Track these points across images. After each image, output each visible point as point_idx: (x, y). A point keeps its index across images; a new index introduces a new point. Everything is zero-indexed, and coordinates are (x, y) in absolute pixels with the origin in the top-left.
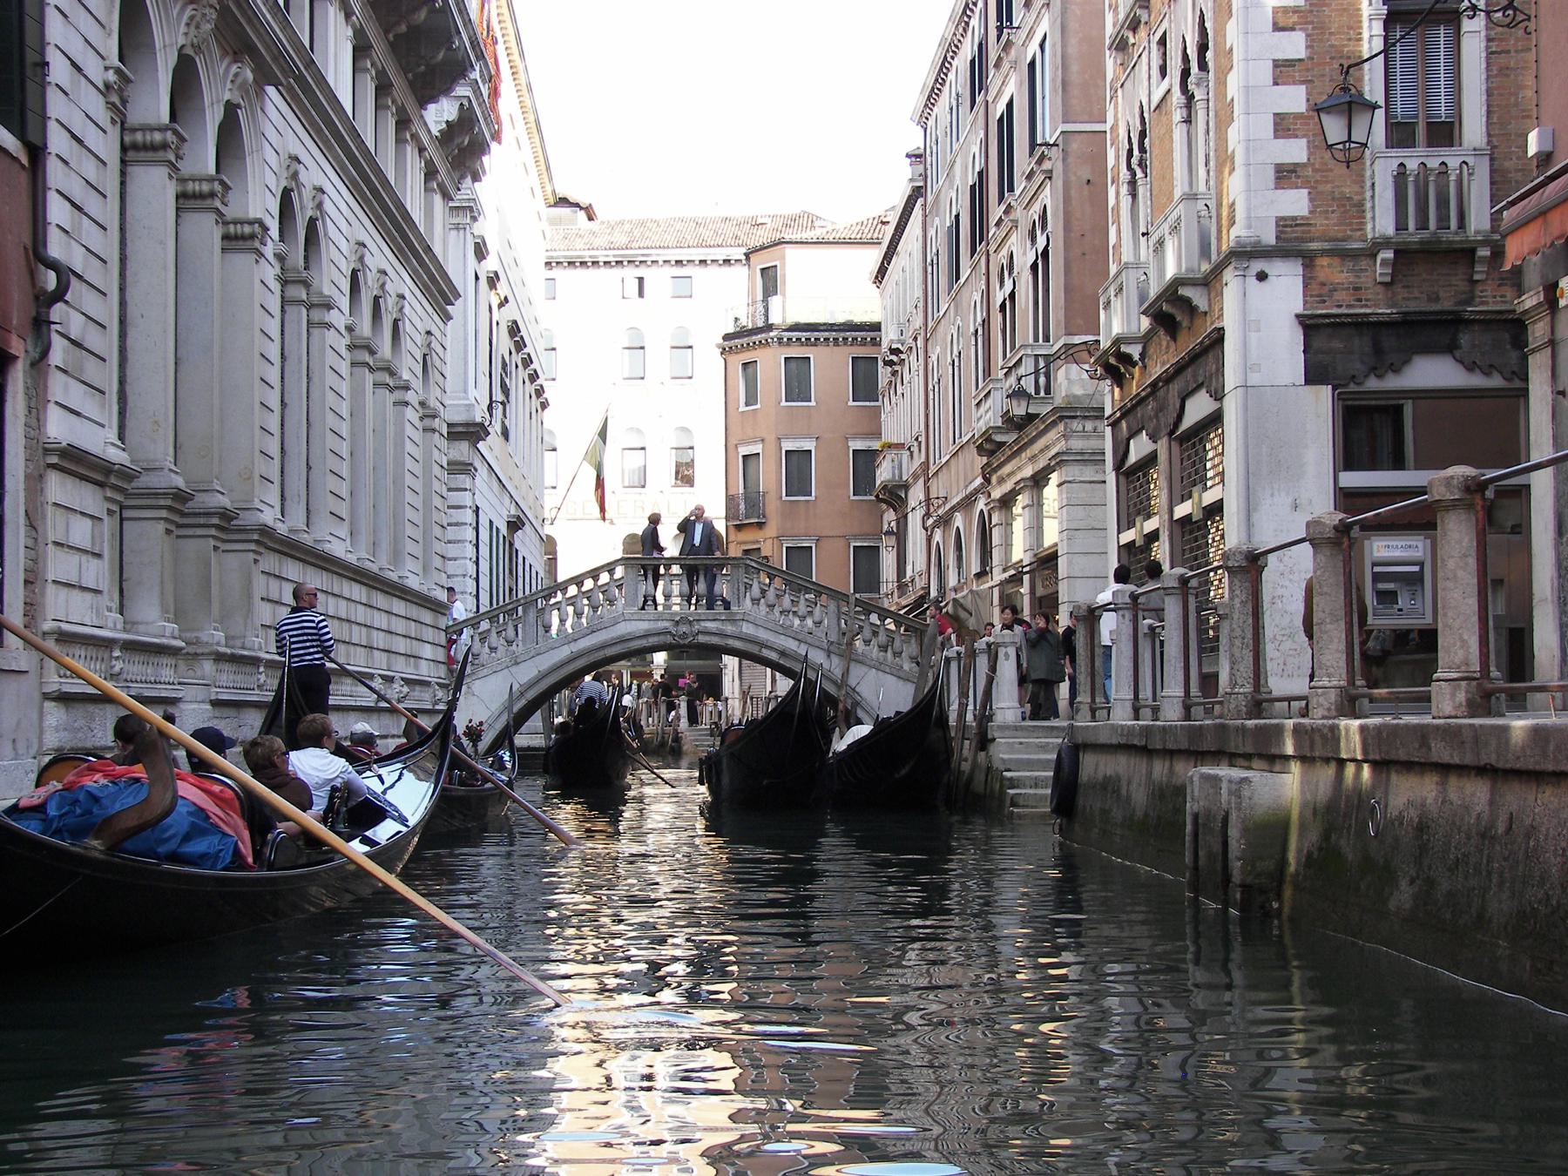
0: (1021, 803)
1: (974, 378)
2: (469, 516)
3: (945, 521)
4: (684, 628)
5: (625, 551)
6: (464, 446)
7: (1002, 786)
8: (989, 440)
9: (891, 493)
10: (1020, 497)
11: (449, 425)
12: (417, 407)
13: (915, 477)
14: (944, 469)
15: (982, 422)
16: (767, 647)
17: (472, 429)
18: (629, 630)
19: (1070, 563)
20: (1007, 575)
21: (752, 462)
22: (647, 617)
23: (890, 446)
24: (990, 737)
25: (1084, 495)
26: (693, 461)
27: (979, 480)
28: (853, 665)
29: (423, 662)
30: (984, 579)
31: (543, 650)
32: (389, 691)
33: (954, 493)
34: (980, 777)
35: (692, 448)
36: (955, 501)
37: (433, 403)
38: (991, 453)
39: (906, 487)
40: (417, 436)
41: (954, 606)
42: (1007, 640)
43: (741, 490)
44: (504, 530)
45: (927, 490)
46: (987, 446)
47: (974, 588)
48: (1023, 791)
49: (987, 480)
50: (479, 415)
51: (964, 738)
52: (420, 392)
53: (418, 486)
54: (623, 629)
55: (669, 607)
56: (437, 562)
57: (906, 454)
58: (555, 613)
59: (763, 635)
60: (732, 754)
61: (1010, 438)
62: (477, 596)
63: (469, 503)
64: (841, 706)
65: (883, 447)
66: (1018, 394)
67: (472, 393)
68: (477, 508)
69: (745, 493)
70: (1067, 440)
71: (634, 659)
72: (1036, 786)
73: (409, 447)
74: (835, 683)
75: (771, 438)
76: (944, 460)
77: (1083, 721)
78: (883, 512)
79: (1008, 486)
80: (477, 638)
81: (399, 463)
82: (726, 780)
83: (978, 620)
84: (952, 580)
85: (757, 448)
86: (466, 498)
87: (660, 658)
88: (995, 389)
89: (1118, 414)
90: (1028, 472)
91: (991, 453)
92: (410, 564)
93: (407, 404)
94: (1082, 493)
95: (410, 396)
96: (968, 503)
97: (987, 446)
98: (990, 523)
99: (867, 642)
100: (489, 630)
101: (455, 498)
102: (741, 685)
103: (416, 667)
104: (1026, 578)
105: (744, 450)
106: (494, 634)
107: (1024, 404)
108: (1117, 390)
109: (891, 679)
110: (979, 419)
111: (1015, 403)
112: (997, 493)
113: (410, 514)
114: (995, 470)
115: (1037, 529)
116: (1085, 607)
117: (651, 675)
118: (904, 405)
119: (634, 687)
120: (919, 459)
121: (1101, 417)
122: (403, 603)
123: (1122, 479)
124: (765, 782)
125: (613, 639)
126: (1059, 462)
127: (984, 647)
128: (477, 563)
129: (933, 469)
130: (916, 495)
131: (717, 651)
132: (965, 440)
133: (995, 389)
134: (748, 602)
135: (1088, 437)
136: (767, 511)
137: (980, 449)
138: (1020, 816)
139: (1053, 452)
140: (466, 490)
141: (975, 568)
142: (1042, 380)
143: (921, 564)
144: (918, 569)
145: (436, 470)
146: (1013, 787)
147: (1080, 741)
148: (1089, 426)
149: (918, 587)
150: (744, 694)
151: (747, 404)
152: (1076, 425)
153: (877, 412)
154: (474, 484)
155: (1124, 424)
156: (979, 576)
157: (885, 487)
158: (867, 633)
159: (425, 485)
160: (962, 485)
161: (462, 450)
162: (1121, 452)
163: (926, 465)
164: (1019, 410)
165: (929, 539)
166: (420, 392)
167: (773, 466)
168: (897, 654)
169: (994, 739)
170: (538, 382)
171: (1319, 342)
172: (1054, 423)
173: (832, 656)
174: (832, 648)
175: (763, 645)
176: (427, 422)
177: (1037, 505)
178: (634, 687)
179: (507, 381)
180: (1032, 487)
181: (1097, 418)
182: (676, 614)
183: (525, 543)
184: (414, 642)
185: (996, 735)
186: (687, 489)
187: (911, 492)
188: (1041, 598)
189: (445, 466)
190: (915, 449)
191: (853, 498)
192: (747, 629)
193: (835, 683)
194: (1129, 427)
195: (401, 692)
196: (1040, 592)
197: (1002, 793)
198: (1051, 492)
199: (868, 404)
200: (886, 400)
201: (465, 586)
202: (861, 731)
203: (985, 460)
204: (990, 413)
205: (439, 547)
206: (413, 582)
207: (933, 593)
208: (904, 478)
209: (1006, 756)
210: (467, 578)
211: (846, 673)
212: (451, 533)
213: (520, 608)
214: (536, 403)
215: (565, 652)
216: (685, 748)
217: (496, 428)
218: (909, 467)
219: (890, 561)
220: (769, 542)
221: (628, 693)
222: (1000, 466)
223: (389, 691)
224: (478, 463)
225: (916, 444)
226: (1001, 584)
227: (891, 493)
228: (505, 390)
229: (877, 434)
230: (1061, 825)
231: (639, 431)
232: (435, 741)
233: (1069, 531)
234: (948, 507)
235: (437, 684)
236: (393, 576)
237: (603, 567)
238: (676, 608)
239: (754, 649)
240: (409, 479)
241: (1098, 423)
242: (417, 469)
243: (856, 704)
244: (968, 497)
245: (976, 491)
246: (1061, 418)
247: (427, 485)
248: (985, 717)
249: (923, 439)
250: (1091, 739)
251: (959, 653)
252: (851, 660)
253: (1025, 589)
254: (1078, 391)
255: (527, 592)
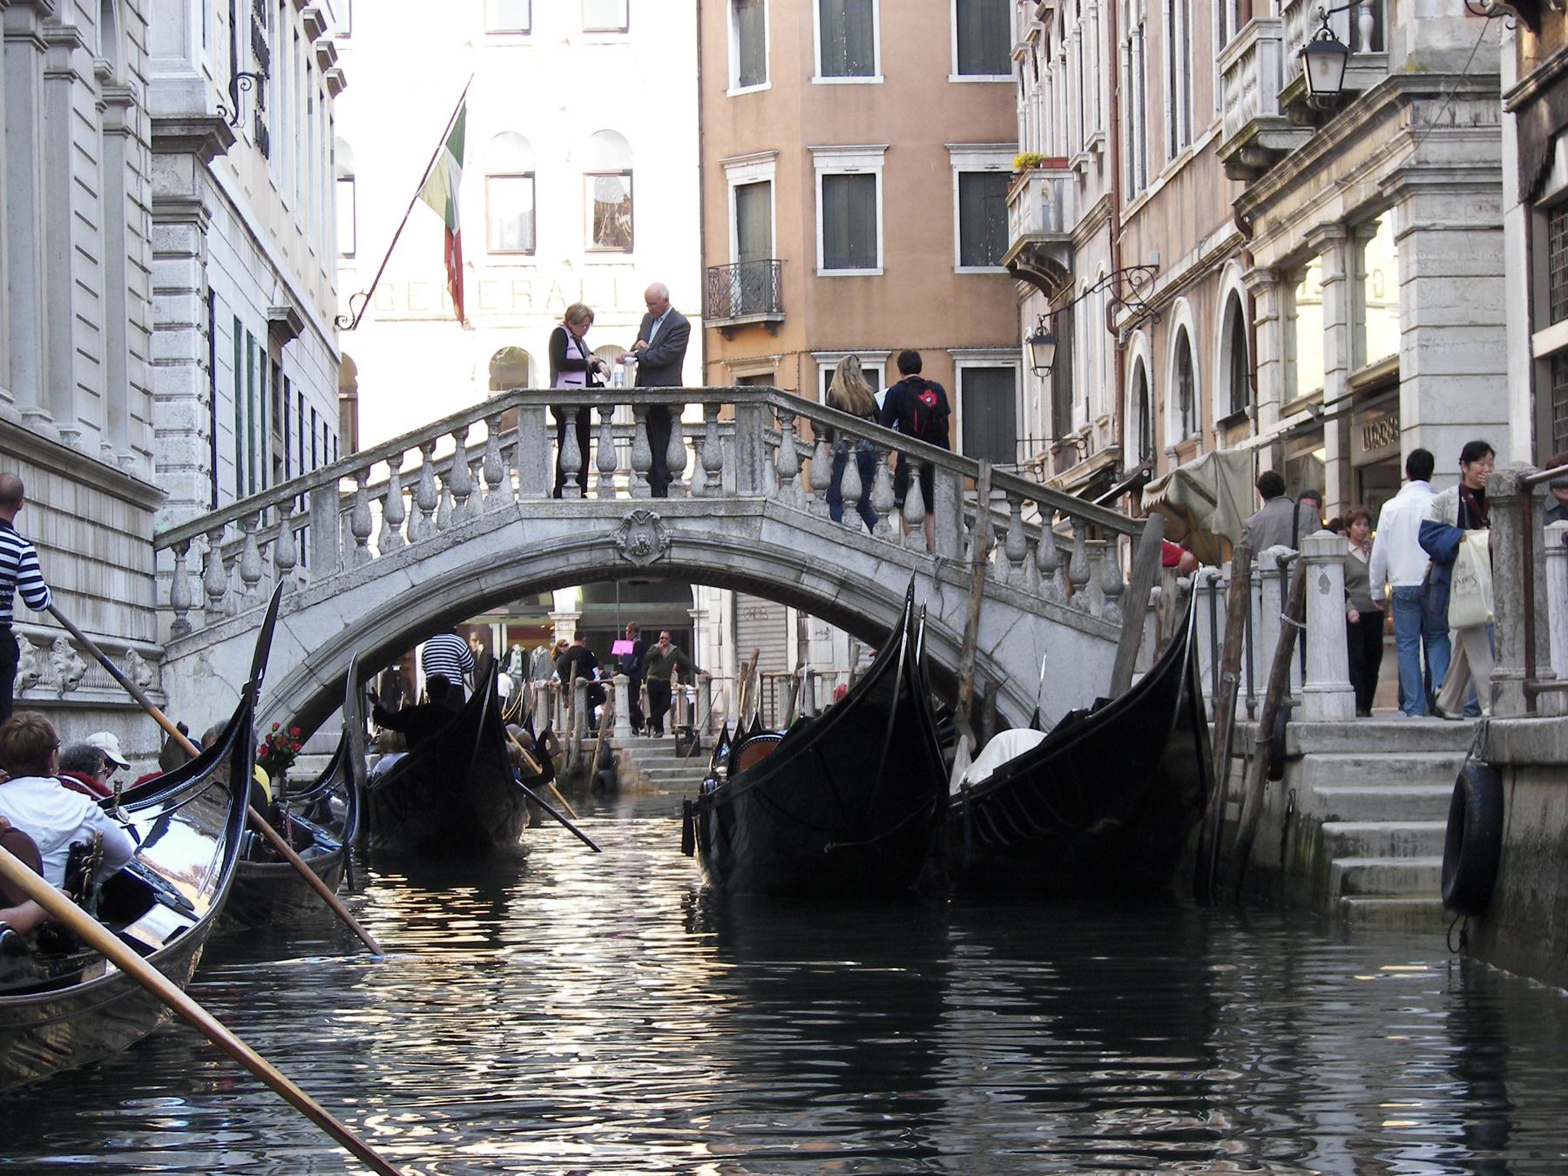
0: (1364, 886)
1: (1215, 20)
2: (194, 309)
3: (1155, 315)
4: (641, 535)
5: (495, 384)
6: (184, 165)
7: (1320, 851)
8: (1252, 146)
9: (1040, 259)
10: (1318, 260)
11: (156, 123)
12: (91, 81)
13: (1091, 225)
14: (1153, 209)
15: (1236, 111)
16: (811, 571)
17: (198, 131)
18: (530, 540)
19: (1425, 395)
20: (1291, 422)
21: (754, 200)
22: (566, 512)
23: (1037, 163)
24: (1290, 750)
25: (1453, 255)
26: (629, 200)
27: (1229, 230)
28: (987, 606)
29: (111, 608)
30: (1239, 430)
31: (354, 581)
32: (46, 669)
33: (1174, 257)
34: (1269, 835)
35: (627, 173)
36: (1175, 274)
37: (122, 75)
38: (1256, 173)
39: (1071, 246)
40: (92, 142)
41: (1180, 487)
42: (1325, 551)
43: (733, 257)
44: (262, 338)
45: (1116, 252)
46: (1249, 159)
47: (1219, 449)
48: (1366, 862)
49: (1246, 229)
50: (213, 101)
51: (1231, 754)
52: (98, 52)
53: (96, 247)
54: (517, 537)
55: (611, 491)
56: (136, 402)
57: (1070, 181)
58: (376, 506)
59: (803, 546)
60: (756, 790)
61: (1295, 141)
62: (213, 474)
63: (195, 283)
64: (963, 691)
65: (1024, 165)
66: (1323, 48)
67: (198, 56)
68: (212, 293)
69: (742, 262)
70: (1417, 144)
71: (515, 603)
72: (1393, 851)
73: (77, 165)
74: (950, 643)
75: (793, 151)
76: (1152, 190)
77: (1509, 716)
78: (1023, 299)
79: (1290, 241)
80: (217, 558)
81: (59, 200)
82: (741, 844)
83: (1229, 519)
84: (1170, 433)
85: (765, 171)
86: (188, 274)
87: (568, 600)
88: (1265, 41)
89: (1532, 87)
90: (1334, 210)
91: (1256, 173)
92: (83, 407)
93: (70, 76)
94: (1449, 250)
95: (78, 60)
96: (1203, 276)
97: (1249, 159)
98: (1253, 315)
99: (1015, 560)
100: (241, 543)
101: (168, 271)
102: (736, 652)
103: (98, 617)
104: (1331, 428)
105: (739, 175)
106: (252, 549)
107: (1335, 67)
108: (1528, 38)
109: (1065, 636)
110: (1230, 104)
111: (1316, 66)
112: (1267, 256)
113: (80, 303)
114: (1262, 209)
115: (1352, 325)
116: (1511, 479)
117: (546, 634)
118: (1064, 81)
119: (516, 659)
120: (1099, 189)
121: (1494, 96)
122: (69, 487)
123: (1539, 220)
124: (827, 848)
125: (497, 557)
126: (1401, 188)
127: (1273, 565)
128: (212, 405)
129: (1128, 209)
130: (1092, 263)
131: (679, 581)
132: (1197, 147)
133: (1265, 41)
134: (769, 483)
135: (1461, 137)
136: (787, 302)
137: (1233, 165)
138: (1363, 914)
139: (1389, 167)
140: (188, 255)
141: (1220, 408)
142: (1365, 20)
143: (1104, 403)
144: (1097, 413)
145: (132, 214)
146: (1345, 854)
147: (1505, 756)
148: (1464, 113)
149: (1098, 449)
150: (747, 672)
151: (744, 81)
152: (1436, 112)
153: (1006, 98)
154: (204, 243)
155: (1543, 107)
156: (1228, 424)
157: (1028, 248)
158: (1016, 541)
159: (109, 246)
160: (1190, 242)
161: (179, 174)
162: (1534, 174)
163: (1113, 202)
164: (1325, 79)
165: (1121, 352)
166: (98, 52)
167: (796, 210)
168: (1074, 586)
169: (1299, 757)
170: (326, 36)
171: (523, 380)
172: (1391, 110)
173: (946, 589)
174: (945, 573)
175: (803, 567)
176: (113, 114)
177: (1353, 278)
178: (516, 659)
179: (265, 33)
180: (1342, 242)
181: (1480, 96)
182: (625, 505)
183: (300, 360)
184: (92, 566)
185: (1305, 746)
186: (619, 257)
187: (1082, 257)
188: (1361, 470)
189: (148, 204)
190: (1090, 170)
191: (960, 270)
192: (771, 535)
193: (950, 643)
194: (1554, 115)
195: (68, 669)
196: (1360, 455)
197: (1322, 868)
198: (1381, 252)
199: (989, 78)
200: (1028, 71)
201: (189, 451)
202: (1018, 741)
203: (1240, 188)
204: (1255, 92)
205: (137, 372)
206: (89, 444)
207: (1131, 462)
208: (1068, 228)
209: (1327, 791)
210: (194, 437)
211: (973, 623)
212: (161, 344)
213: (271, 511)
214: (319, 80)
215: (398, 586)
216: (625, 780)
217: (245, 130)
218: (1078, 207)
219: (1038, 398)
220: (791, 362)
221: (504, 670)
222: (1274, 200)
223: (46, 669)
224: (211, 201)
225: (1091, 158)
226: (1278, 442)
227: (1040, 259)
228: (261, 53)
229: (1007, 140)
230: (1463, 934)
231: (520, 138)
232: (219, 771)
233: (1425, 330)
234: (1161, 285)
235: (142, 653)
236: (51, 431)
237: (475, 410)
238: (622, 496)
239: (785, 576)
240: (78, 233)
241: (1482, 107)
242: (94, 211)
243: (995, 686)
244: (1203, 265)
245: (1223, 252)
246: (1407, 98)
247: (115, 245)
248: (1280, 706)
249: (1106, 148)
250: (1535, 753)
251: (1212, 582)
252: (983, 596)
253: (1326, 453)
254: (1440, 41)
255: (320, 466)
